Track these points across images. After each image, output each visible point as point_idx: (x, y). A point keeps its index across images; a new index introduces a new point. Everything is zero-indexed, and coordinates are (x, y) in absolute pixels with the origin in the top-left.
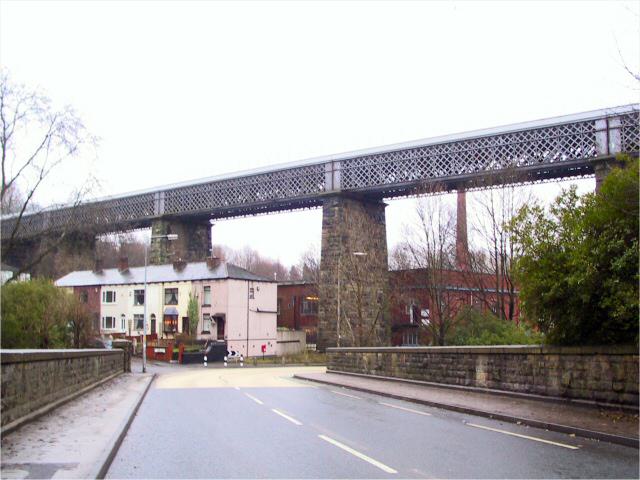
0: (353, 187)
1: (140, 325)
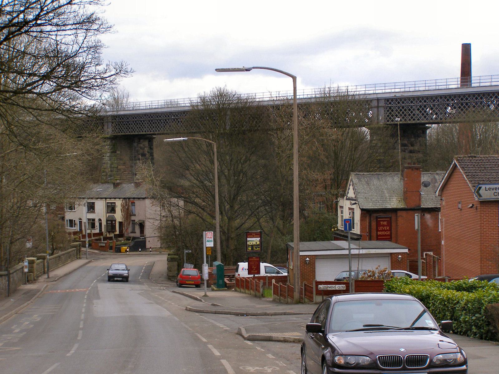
1: (93, 226)
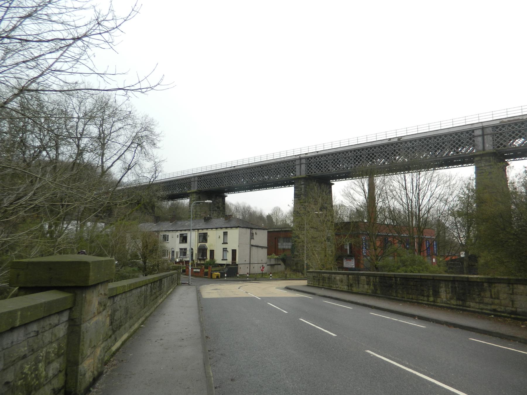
0: (313, 173)
